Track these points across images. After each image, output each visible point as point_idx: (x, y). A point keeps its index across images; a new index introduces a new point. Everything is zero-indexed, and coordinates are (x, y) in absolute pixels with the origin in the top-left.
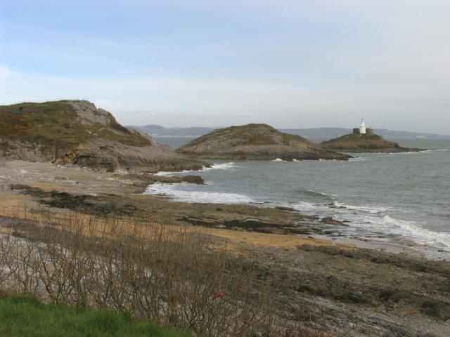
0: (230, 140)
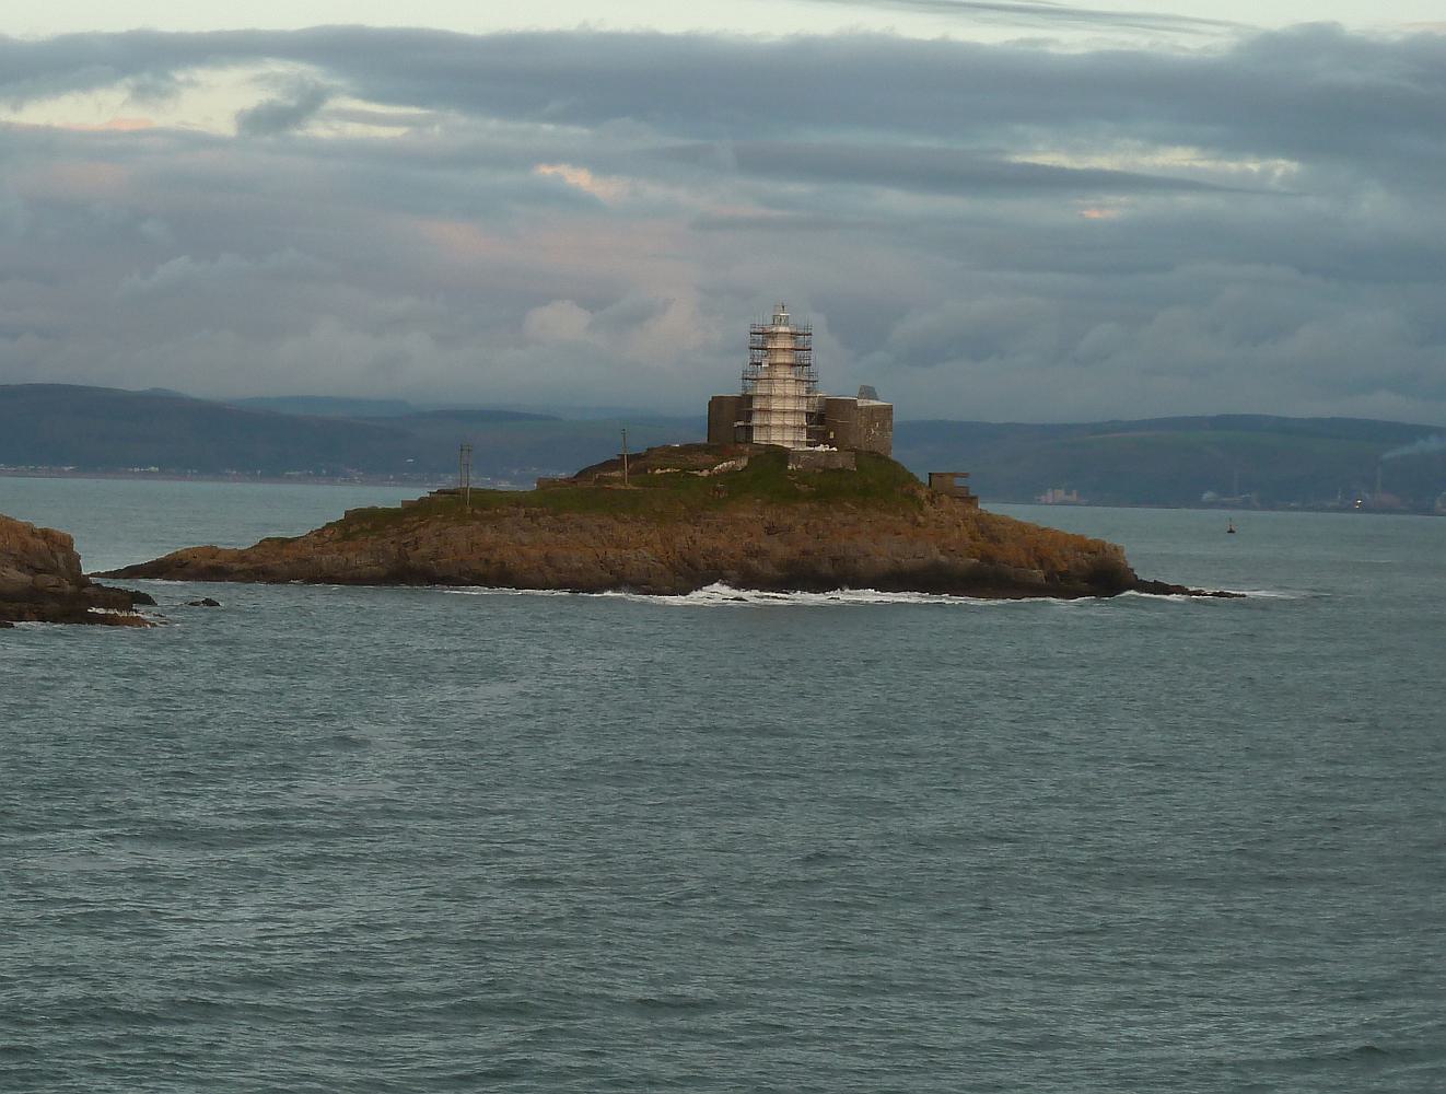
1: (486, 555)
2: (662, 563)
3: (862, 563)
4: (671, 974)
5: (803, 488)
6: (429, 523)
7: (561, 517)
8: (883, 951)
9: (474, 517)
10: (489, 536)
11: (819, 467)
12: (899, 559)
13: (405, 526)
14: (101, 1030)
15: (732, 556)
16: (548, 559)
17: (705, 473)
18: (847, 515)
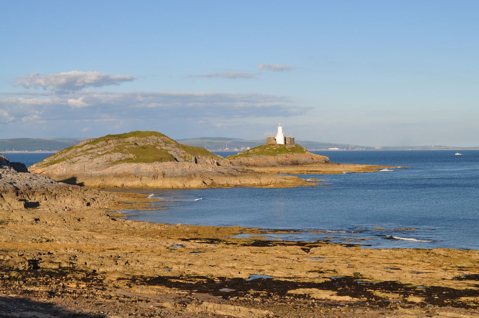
0: (108, 156)
17: (275, 148)
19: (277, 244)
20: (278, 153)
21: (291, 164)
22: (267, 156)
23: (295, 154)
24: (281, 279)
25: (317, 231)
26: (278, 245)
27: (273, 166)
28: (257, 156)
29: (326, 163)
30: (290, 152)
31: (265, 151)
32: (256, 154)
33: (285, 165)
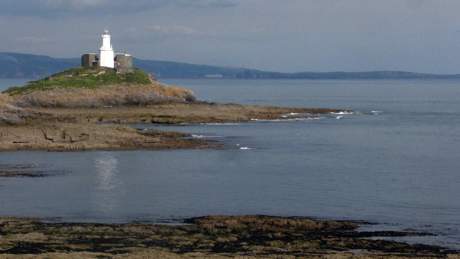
1: (52, 99)
2: (96, 100)
3: (142, 98)
4: (342, 117)
5: (122, 78)
6: (35, 91)
7: (67, 88)
8: (25, 249)
9: (46, 89)
10: (51, 94)
11: (125, 73)
12: (151, 97)
13: (28, 92)
14: (316, 117)
15: (111, 97)
16: (69, 99)
17: (96, 75)
18: (135, 85)
19: (57, 248)
20: (101, 84)
21: (124, 104)
22: (80, 88)
23: (133, 86)
24: (375, 251)
25: (369, 255)
26: (57, 250)
27: (93, 107)
28: (63, 89)
29: (188, 102)
30: (124, 81)
31: (78, 79)
32: (61, 85)
33: (114, 105)
